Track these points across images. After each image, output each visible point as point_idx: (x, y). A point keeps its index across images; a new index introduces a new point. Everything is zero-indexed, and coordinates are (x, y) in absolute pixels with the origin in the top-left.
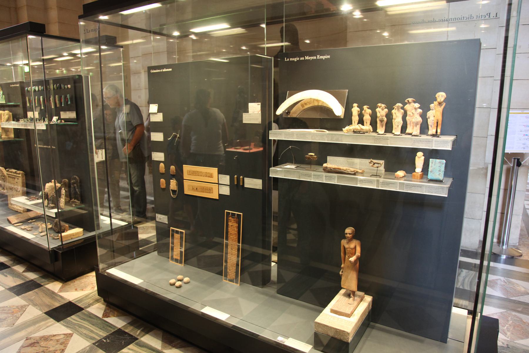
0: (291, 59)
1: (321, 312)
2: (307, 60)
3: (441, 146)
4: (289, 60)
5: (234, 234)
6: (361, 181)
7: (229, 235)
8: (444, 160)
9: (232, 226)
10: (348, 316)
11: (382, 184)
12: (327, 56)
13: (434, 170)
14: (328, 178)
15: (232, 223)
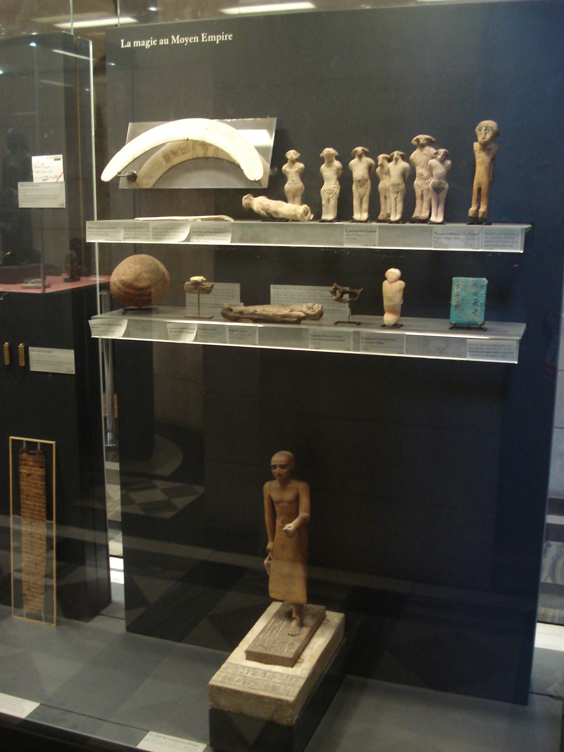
0: (137, 44)
1: (223, 659)
2: (175, 45)
3: (500, 244)
4: (132, 44)
5: (36, 497)
6: (318, 338)
7: (22, 501)
8: (484, 279)
9: (31, 477)
10: (293, 661)
11: (366, 343)
12: (226, 36)
13: (464, 302)
14: (236, 333)
15: (27, 467)
